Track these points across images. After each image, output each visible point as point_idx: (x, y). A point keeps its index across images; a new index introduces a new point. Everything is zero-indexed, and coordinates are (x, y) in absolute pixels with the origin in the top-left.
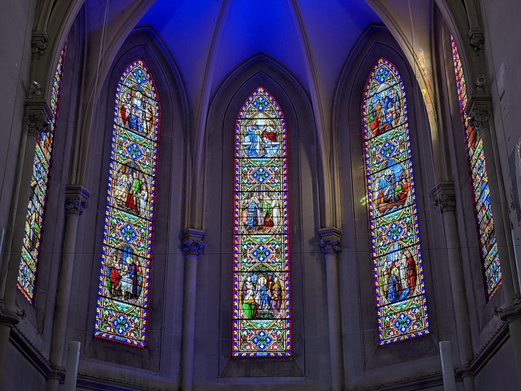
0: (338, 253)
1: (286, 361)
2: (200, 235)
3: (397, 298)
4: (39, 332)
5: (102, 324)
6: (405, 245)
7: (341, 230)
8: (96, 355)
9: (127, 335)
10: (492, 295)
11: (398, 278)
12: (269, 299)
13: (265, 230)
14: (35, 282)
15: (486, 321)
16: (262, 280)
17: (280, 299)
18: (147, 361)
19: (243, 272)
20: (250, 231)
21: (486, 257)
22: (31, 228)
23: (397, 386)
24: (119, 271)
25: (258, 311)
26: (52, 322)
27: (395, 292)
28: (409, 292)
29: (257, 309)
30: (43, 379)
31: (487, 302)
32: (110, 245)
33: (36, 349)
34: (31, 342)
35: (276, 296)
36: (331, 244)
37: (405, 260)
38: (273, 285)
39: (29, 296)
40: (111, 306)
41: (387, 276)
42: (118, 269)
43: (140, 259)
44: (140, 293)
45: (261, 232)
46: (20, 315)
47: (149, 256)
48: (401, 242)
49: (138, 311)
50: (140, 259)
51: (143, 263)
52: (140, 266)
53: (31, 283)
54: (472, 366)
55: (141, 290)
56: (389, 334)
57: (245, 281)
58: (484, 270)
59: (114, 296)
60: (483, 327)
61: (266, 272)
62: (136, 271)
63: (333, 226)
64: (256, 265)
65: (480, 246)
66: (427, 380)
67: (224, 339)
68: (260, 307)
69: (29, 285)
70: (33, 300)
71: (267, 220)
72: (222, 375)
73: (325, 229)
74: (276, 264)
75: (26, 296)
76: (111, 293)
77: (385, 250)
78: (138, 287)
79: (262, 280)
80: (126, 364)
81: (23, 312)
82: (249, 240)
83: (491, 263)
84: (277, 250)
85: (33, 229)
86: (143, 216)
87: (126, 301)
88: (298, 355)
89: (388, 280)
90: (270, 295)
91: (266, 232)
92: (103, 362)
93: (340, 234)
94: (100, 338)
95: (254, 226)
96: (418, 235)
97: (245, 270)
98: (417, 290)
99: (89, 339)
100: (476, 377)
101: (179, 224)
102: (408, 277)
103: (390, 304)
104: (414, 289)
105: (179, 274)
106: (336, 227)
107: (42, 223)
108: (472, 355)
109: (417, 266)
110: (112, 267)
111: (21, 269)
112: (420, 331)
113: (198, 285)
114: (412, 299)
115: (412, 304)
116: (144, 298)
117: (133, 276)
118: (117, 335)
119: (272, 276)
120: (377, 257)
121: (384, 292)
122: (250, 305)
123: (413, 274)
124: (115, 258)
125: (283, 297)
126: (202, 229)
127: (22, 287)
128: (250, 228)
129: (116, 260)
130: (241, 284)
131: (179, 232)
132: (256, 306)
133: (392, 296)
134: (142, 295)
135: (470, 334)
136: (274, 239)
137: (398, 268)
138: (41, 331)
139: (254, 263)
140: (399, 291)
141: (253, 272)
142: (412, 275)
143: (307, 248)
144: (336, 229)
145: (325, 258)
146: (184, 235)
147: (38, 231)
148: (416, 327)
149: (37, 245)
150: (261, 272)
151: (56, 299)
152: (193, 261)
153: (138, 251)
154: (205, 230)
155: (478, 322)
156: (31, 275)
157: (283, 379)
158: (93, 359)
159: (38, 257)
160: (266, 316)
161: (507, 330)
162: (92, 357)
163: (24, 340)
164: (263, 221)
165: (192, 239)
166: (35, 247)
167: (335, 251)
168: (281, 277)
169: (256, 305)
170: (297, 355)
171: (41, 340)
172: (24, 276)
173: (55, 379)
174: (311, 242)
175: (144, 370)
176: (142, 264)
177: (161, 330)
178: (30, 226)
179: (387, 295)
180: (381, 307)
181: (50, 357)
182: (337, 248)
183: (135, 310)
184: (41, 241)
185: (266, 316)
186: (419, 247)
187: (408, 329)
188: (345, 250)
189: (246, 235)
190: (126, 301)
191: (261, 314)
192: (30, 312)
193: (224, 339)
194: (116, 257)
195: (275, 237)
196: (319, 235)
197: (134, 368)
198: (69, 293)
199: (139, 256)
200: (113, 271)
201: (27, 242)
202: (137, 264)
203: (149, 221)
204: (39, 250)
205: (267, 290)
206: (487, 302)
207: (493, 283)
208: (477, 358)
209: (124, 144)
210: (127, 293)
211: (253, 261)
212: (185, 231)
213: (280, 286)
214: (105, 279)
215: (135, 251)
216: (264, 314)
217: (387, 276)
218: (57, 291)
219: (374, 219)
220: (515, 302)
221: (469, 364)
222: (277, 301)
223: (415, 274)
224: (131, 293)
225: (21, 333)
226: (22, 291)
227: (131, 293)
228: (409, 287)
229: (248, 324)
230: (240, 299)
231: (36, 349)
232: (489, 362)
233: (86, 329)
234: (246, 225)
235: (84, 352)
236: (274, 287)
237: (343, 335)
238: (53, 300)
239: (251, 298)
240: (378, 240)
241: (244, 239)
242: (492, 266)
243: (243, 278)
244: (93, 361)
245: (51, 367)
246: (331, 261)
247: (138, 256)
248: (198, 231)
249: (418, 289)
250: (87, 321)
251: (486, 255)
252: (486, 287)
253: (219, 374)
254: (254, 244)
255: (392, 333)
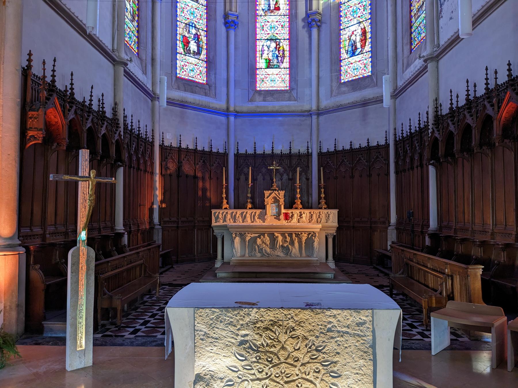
0: (319, 27)
1: (286, 93)
2: (235, 16)
3: (353, 54)
4: (144, 73)
5: (181, 70)
6: (361, 20)
7: (322, 12)
8: (179, 88)
9: (196, 77)
10: (415, 49)
11: (355, 42)
12: (277, 56)
13: (275, 13)
14: (138, 42)
15: (408, 65)
16: (273, 45)
17: (283, 56)
18: (208, 92)
19: (262, 40)
20: (266, 13)
21: (413, 25)
22: (130, 6)
23: (350, 105)
24: (188, 38)
25: (271, 63)
26: (151, 68)
27: (353, 50)
28: (361, 50)
29: (270, 62)
30: (150, 101)
31: (410, 54)
32: (182, 21)
33: (142, 83)
34: (139, 78)
35: (281, 54)
36: (315, 21)
37: (361, 30)
38: (279, 48)
39: (135, 51)
40: (185, 59)
41: (349, 40)
42: (187, 37)
43: (200, 31)
44: (201, 52)
45: (272, 14)
46: (129, 61)
47: (205, 29)
48: (358, 18)
49: (201, 63)
50: (200, 31)
51: (203, 34)
52: (200, 35)
53: (135, 43)
54: (395, 94)
55: (202, 50)
56: (347, 76)
57: (263, 46)
58: (411, 33)
59: (186, 53)
60: (406, 69)
61: (275, 39)
62: (198, 38)
63: (317, 9)
64: (269, 35)
65: (411, 17)
66: (368, 102)
67: (251, 80)
68: (272, 61)
69: (134, 44)
70: (138, 53)
71: (276, 6)
72: (251, 100)
73: (312, 11)
74: (282, 34)
75: (133, 51)
76: (184, 51)
77: (348, 24)
78: (200, 48)
79: (273, 45)
80: (196, 93)
81: (131, 58)
82: (265, 19)
83: (417, 28)
84: (282, 26)
85: (132, 7)
86: (200, 3)
87: (193, 57)
88: (293, 89)
89: (349, 43)
90: (278, 54)
91: (275, 14)
92: (183, 92)
93: (321, 15)
94: (180, 78)
95: (268, 10)
96: (370, 13)
97: (263, 39)
98: (365, 49)
99: (174, 78)
100: (398, 100)
101: (223, 8)
102: (362, 41)
103: (348, 58)
104: (364, 48)
105: (224, 41)
106: (319, 10)
107: (138, 4)
108: (396, 87)
109: (367, 33)
110: (184, 36)
111: (127, 33)
112: (365, 73)
113: (236, 48)
114: (363, 55)
115: (362, 57)
116: (204, 55)
117: (197, 41)
118: (190, 77)
119: (279, 42)
120: (343, 29)
121: (346, 51)
122: (266, 60)
123: (364, 39)
124: (185, 30)
125: (285, 55)
126: (236, 12)
127: (130, 45)
128: (266, 12)
129: (186, 31)
130: (261, 47)
131: (223, 14)
132: (269, 61)
133: (351, 53)
134: (203, 53)
135: (397, 74)
136: (281, 18)
137: (356, 35)
138: (145, 73)
139: (268, 34)
140: (355, 50)
141: (267, 39)
142: (364, 40)
143: (300, 24)
144: (319, 11)
145: (311, 30)
146: (226, 16)
147: (135, 9)
148: (363, 71)
149: (136, 18)
150: (273, 40)
151: (152, 54)
152: (232, 33)
153: (199, 26)
154: (239, 13)
155: (403, 67)
156: (135, 38)
157: (285, 102)
158: (178, 90)
159: (138, 26)
160: (275, 67)
161: (426, 67)
162: (176, 89)
163: (134, 76)
164: (274, 7)
165: (231, 18)
166: (135, 19)
167: (317, 25)
168: (284, 43)
169: (270, 60)
170: (293, 89)
171: (146, 78)
172: (130, 38)
173: (156, 101)
174: (303, 20)
175: (207, 97)
176: (202, 34)
177: (215, 74)
178: (130, 5)
179: (347, 52)
180: (343, 60)
181: (152, 89)
182: (319, 24)
183: (199, 62)
184: (138, 16)
185: (275, 67)
186: (370, 21)
187: (358, 73)
188: (324, 26)
189: (264, 16)
190: (193, 57)
191: (272, 65)
192: (135, 59)
193: (251, 80)
194: (186, 29)
195: (281, 17)
196: (308, 15)
197: (201, 96)
198: (159, 50)
199: (200, 29)
200: (185, 38)
201: (129, 15)
202: (199, 34)
203: (205, 6)
204: (138, 21)
205: (276, 51)
206: (410, 54)
207: (416, 41)
208: (399, 88)
209: (185, 66)
210: (194, 52)
211: (268, 33)
212: (227, 13)
213: (284, 48)
214: (180, 43)
215: (197, 26)
216: (274, 66)
217: (349, 40)
218: (152, 49)
219: (342, 4)
220: (435, 50)
221: (394, 92)
222: (282, 57)
223: (365, 39)
224: (196, 52)
225: (131, 72)
226: (130, 47)
227: (196, 52)
228: (361, 47)
229: (265, 71)
230: (260, 56)
231: (142, 83)
232: (408, 90)
233: (172, 73)
234: (263, 10)
235: (172, 86)
236: (280, 49)
237: (320, 77)
238: (150, 55)
239: (267, 56)
240: (344, 18)
241: (262, 19)
242: (417, 30)
243: (262, 44)
244: (177, 91)
245: (154, 94)
246: (315, 31)
247: (199, 29)
248: (234, 13)
249: (368, 48)
250: (172, 68)
251: (414, 23)
252: (411, 44)
253: (249, 100)
254: (268, 22)
255: (348, 75)
